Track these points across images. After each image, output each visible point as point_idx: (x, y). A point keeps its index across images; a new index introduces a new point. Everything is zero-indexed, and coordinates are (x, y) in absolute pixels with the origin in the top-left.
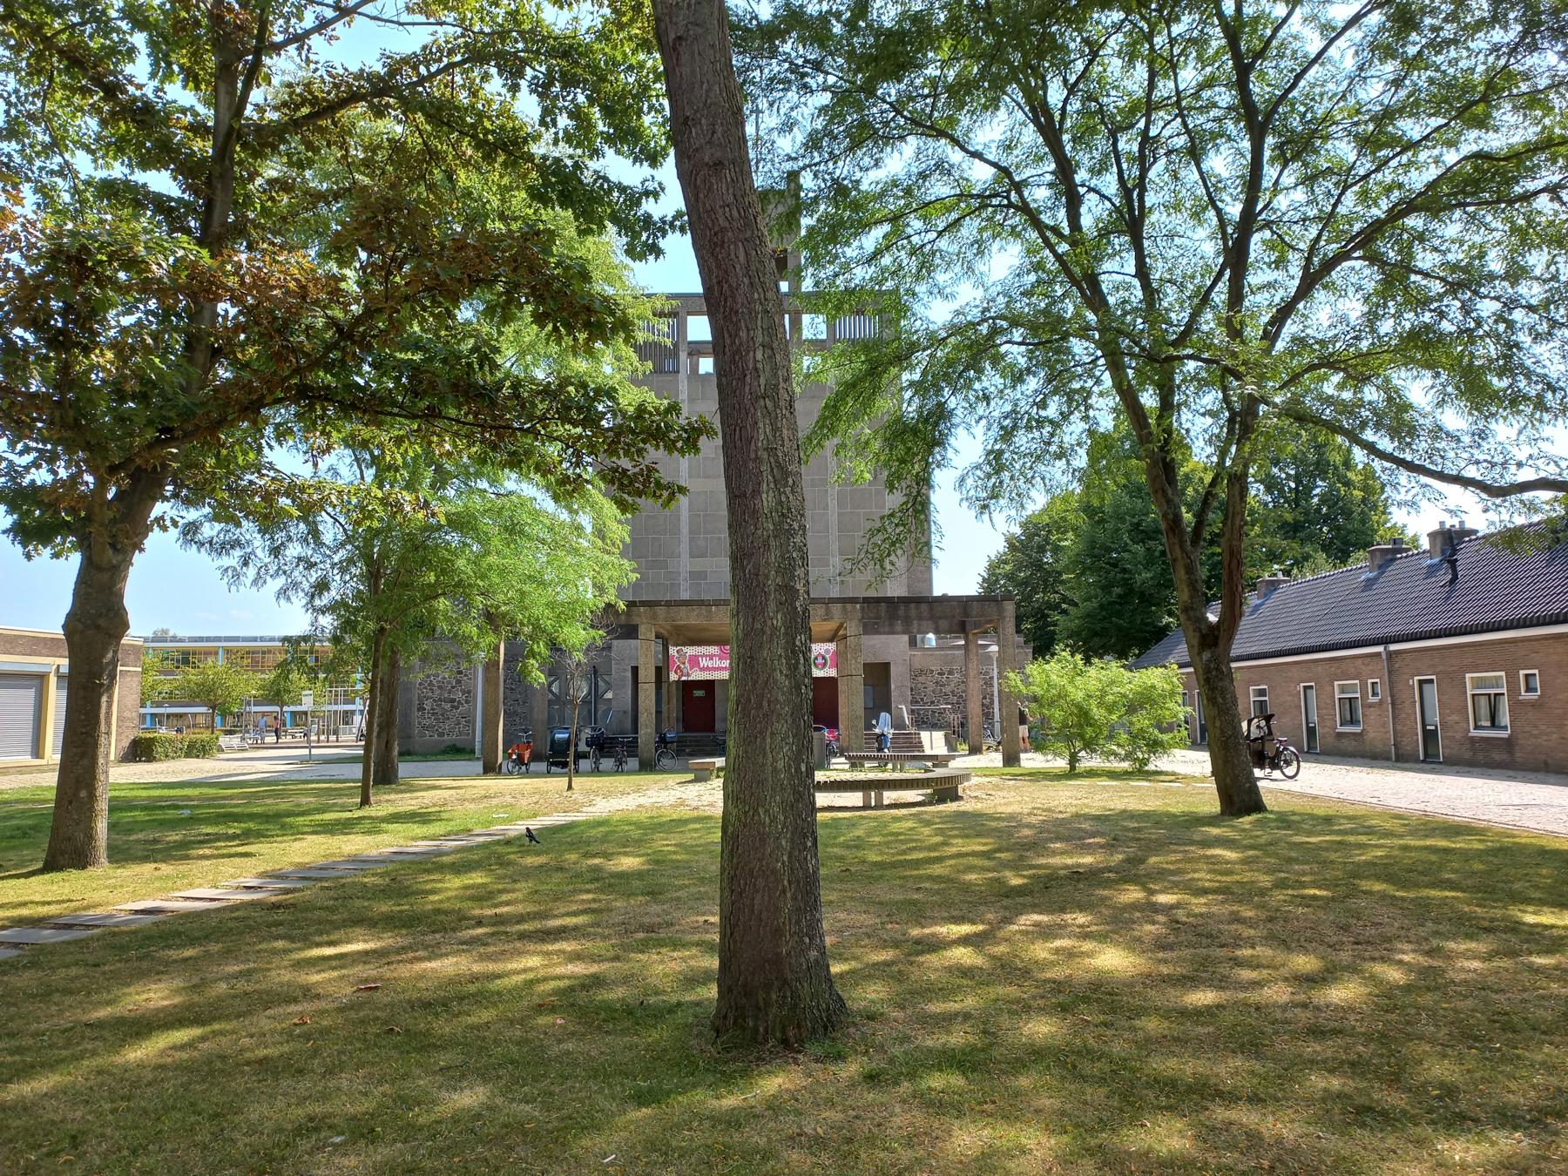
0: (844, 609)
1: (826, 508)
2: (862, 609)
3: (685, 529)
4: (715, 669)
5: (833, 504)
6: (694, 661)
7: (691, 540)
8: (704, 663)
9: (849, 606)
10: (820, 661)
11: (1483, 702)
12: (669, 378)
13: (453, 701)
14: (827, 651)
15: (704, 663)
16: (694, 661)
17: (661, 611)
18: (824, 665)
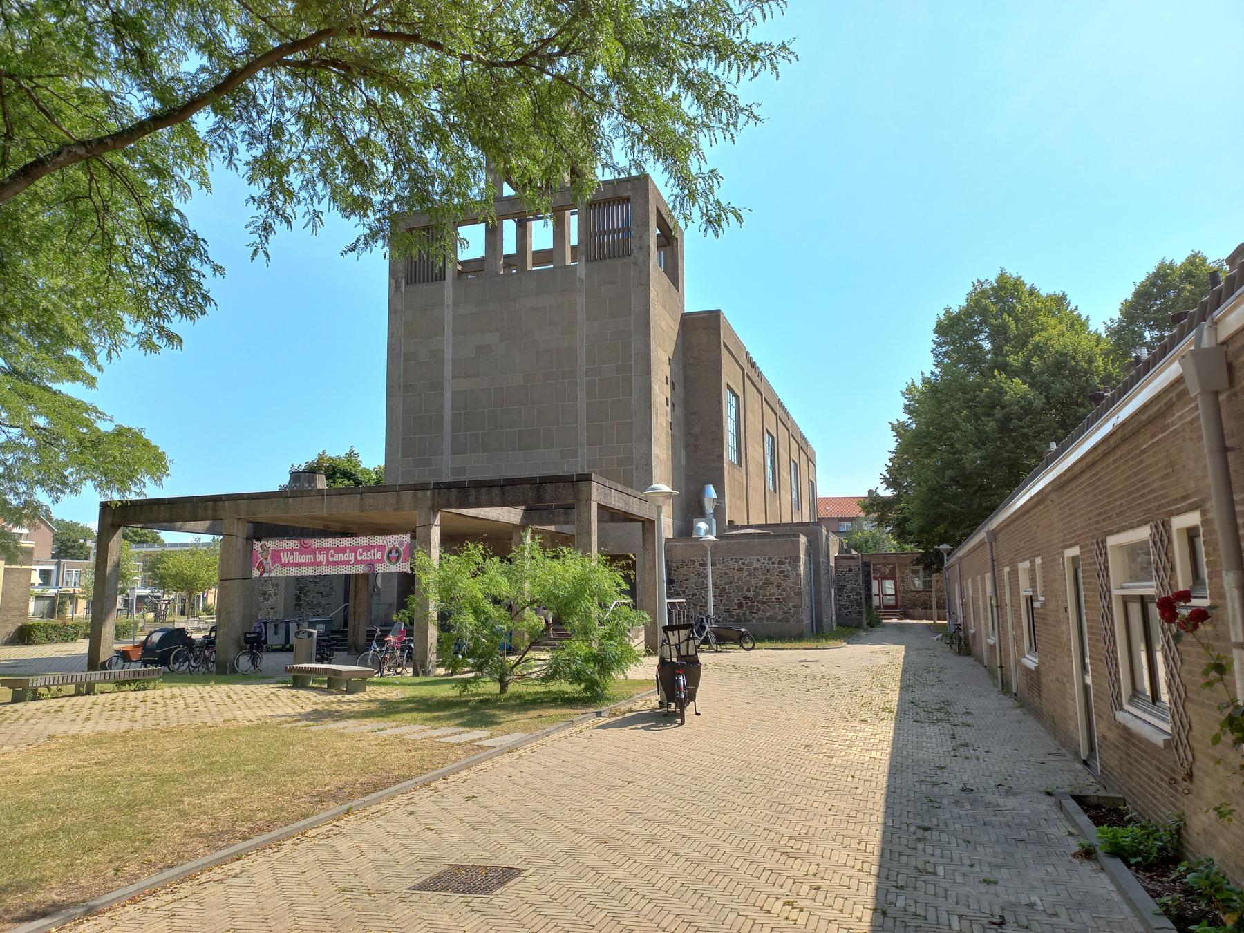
0: (415, 496)
1: (575, 399)
2: (433, 497)
3: (447, 428)
4: (305, 564)
5: (582, 395)
6: (276, 556)
7: (453, 437)
8: (285, 558)
9: (420, 493)
10: (394, 554)
11: (1135, 609)
12: (436, 285)
13: (265, 593)
14: (401, 544)
15: (285, 558)
16: (276, 556)
17: (243, 504)
18: (398, 559)
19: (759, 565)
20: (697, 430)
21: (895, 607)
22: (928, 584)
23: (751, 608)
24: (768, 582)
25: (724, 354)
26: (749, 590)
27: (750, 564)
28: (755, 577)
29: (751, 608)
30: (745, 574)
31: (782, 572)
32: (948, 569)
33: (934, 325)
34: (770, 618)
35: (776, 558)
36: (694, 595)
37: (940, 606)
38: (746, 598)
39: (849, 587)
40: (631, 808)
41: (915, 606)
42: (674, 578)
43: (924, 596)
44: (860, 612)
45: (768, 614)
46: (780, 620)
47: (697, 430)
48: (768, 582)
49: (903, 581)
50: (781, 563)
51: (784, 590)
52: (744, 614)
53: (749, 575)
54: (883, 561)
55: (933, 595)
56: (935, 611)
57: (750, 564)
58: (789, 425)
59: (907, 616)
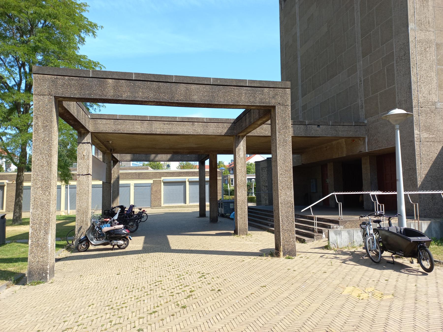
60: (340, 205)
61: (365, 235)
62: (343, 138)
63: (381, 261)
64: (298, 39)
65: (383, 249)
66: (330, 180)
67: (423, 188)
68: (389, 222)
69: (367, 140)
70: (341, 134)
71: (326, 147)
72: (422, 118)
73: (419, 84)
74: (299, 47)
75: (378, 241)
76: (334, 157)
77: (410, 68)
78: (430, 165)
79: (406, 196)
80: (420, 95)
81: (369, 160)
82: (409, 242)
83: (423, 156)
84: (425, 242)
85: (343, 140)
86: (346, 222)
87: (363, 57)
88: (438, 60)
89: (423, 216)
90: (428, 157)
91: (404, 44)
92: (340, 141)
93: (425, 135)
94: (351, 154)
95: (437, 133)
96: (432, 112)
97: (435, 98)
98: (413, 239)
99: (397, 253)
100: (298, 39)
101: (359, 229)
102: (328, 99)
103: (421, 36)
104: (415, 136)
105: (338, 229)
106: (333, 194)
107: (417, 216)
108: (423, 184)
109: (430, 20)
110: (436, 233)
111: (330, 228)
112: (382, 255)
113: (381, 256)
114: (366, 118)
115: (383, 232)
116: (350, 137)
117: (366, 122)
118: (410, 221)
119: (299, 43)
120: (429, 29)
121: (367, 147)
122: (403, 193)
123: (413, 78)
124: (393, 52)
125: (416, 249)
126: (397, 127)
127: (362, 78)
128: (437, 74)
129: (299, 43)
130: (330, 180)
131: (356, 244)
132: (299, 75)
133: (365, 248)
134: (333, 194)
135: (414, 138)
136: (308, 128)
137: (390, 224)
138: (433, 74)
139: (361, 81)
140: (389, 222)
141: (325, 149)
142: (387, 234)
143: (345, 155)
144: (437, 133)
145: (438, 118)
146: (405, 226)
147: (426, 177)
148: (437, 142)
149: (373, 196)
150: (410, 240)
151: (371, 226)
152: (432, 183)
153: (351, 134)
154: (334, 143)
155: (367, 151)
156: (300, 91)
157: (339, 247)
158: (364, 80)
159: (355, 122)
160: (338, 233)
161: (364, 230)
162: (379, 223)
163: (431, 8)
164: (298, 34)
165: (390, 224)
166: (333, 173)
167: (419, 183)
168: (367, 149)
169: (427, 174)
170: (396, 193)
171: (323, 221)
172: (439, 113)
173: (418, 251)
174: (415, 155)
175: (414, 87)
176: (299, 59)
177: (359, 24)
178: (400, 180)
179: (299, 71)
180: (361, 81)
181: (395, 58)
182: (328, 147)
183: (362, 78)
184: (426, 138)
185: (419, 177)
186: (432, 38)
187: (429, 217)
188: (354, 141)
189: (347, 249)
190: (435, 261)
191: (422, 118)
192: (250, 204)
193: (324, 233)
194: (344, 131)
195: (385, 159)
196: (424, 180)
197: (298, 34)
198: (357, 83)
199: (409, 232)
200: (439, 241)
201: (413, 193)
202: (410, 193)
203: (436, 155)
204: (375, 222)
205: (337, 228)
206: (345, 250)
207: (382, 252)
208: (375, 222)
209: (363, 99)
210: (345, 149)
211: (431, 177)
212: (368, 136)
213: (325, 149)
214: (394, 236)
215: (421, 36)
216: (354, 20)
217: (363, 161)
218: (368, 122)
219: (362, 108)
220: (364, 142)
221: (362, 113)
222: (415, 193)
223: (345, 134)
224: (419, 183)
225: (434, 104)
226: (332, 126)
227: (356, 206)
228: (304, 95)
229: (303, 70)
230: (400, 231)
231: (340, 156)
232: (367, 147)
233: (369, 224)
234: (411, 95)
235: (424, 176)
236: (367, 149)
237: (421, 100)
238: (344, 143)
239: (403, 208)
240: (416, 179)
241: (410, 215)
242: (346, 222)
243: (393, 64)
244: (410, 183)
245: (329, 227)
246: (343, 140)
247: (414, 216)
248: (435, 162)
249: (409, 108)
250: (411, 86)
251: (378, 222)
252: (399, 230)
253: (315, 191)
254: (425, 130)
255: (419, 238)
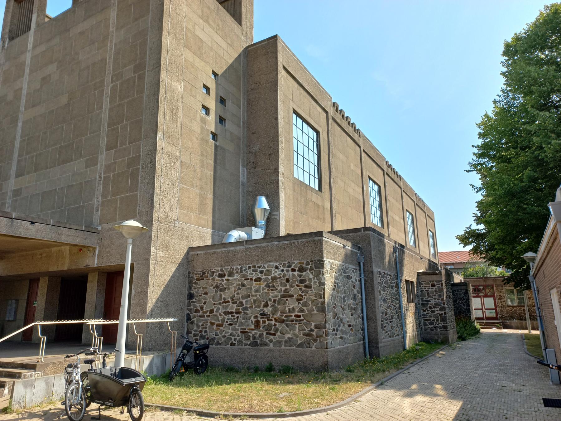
19: (277, 273)
20: (257, 148)
21: (496, 318)
22: (521, 300)
23: (268, 329)
24: (287, 295)
25: (282, 75)
26: (266, 305)
27: (269, 272)
28: (273, 288)
29: (268, 329)
30: (263, 284)
31: (302, 281)
32: (535, 276)
33: (502, 49)
34: (289, 342)
35: (296, 264)
36: (212, 311)
37: (533, 318)
38: (263, 315)
39: (433, 302)
40: (394, 407)
41: (512, 318)
42: (194, 291)
43: (519, 311)
44: (445, 328)
45: (288, 336)
46: (300, 346)
47: (257, 148)
48: (287, 295)
49: (501, 299)
50: (301, 270)
51: (305, 304)
52: (261, 336)
53: (267, 286)
54: (483, 283)
55: (526, 309)
56: (529, 323)
57: (269, 272)
58: (401, 184)
59: (506, 327)
60: (44, 340)
61: (69, 383)
62: (67, 244)
63: (85, 418)
64: (24, 98)
65: (92, 399)
66: (40, 303)
67: (152, 316)
68: (104, 360)
69: (97, 251)
70: (64, 239)
71: (41, 255)
72: (161, 235)
73: (161, 197)
74: (22, 108)
75: (85, 390)
76: (51, 270)
77: (154, 178)
78: (163, 288)
79: (128, 324)
80: (161, 210)
81: (97, 278)
82: (121, 386)
83: (156, 278)
84: (138, 383)
85: (68, 248)
86: (47, 365)
87: (107, 150)
88: (181, 178)
89: (146, 350)
90: (162, 279)
91: (151, 150)
92: (63, 248)
93: (161, 254)
94: (74, 267)
95: (173, 253)
96: (171, 230)
97: (175, 216)
98: (126, 381)
99: (106, 403)
100: (24, 98)
101: (63, 374)
102: (55, 190)
103: (168, 148)
104: (152, 254)
105: (33, 377)
106: (36, 323)
107: (139, 349)
108: (152, 310)
109: (178, 136)
110: (157, 369)
111: (19, 377)
112: (87, 409)
113: (85, 410)
114: (100, 224)
115: (94, 376)
116: (76, 245)
117: (100, 228)
118: (132, 357)
119: (23, 103)
120: (176, 144)
121: (96, 260)
122: (126, 322)
123: (157, 190)
124: (140, 155)
125: (128, 395)
126: (130, 241)
127: (102, 174)
128: (179, 192)
129: (23, 103)
130: (40, 303)
131: (55, 398)
132: (17, 145)
133: (64, 403)
134: (36, 323)
135: (150, 255)
136: (15, 223)
137: (104, 364)
138: (175, 191)
139: (100, 177)
140: (104, 360)
141: (39, 257)
142: (98, 378)
143: (66, 268)
144: (173, 253)
145: (176, 237)
146: (122, 365)
147: (156, 303)
148: (172, 262)
149: (92, 325)
150: (122, 384)
151: (79, 369)
152: (161, 309)
153: (78, 241)
154: (54, 249)
155: (96, 266)
156: (14, 168)
157: (27, 406)
158: (104, 177)
159: (86, 227)
160: (30, 385)
161: (70, 374)
162: (91, 363)
163: (179, 125)
164: (24, 92)
165: (104, 364)
166: (46, 291)
167: (149, 309)
168: (96, 263)
169: (158, 299)
170: (117, 322)
171: (12, 368)
172: (176, 232)
173: (130, 396)
174: (148, 276)
175: (156, 199)
176: (20, 125)
177: (107, 111)
178: (124, 306)
179: (18, 140)
180: (100, 177)
181: (141, 163)
182: (44, 255)
183: (102, 174)
184: (162, 257)
185: (150, 302)
186: (178, 154)
187: (154, 351)
188: (81, 250)
189: (39, 408)
190: (148, 406)
191: (161, 235)
192: (334, 258)
193: (6, 388)
194: (68, 236)
195: (112, 278)
196: (154, 305)
197: (24, 92)
198: (96, 179)
199: (126, 373)
200: (158, 379)
201: (139, 321)
202: (136, 321)
203: (169, 277)
204: (87, 362)
205: (31, 375)
206: (36, 410)
207: (87, 405)
208: (87, 362)
209: (100, 200)
210: (67, 260)
211: (162, 302)
212: (100, 246)
213: (39, 257)
214: (105, 380)
215: (168, 148)
216: (102, 104)
217: (90, 278)
218: (102, 228)
219: (97, 210)
220: (94, 253)
221: (97, 217)
222: (142, 321)
223: (70, 240)
224: (149, 309)
225: (174, 221)
226: (53, 227)
227: (68, 338)
228: (19, 175)
229: (24, 140)
230: (115, 372)
231: (59, 269)
232: (96, 260)
233: (76, 366)
234: (153, 207)
235: (154, 301)
236: (96, 263)
237: (162, 215)
238: (68, 252)
239: (122, 341)
240: (146, 304)
241: (130, 348)
242: (47, 365)
243: (138, 169)
244: (138, 308)
245: (19, 376)
246: (68, 248)
247: (136, 350)
248: (167, 286)
249: (148, 222)
250: (153, 197)
251: (90, 362)
252: (114, 372)
253: (12, 319)
254: (162, 248)
255: (133, 379)
